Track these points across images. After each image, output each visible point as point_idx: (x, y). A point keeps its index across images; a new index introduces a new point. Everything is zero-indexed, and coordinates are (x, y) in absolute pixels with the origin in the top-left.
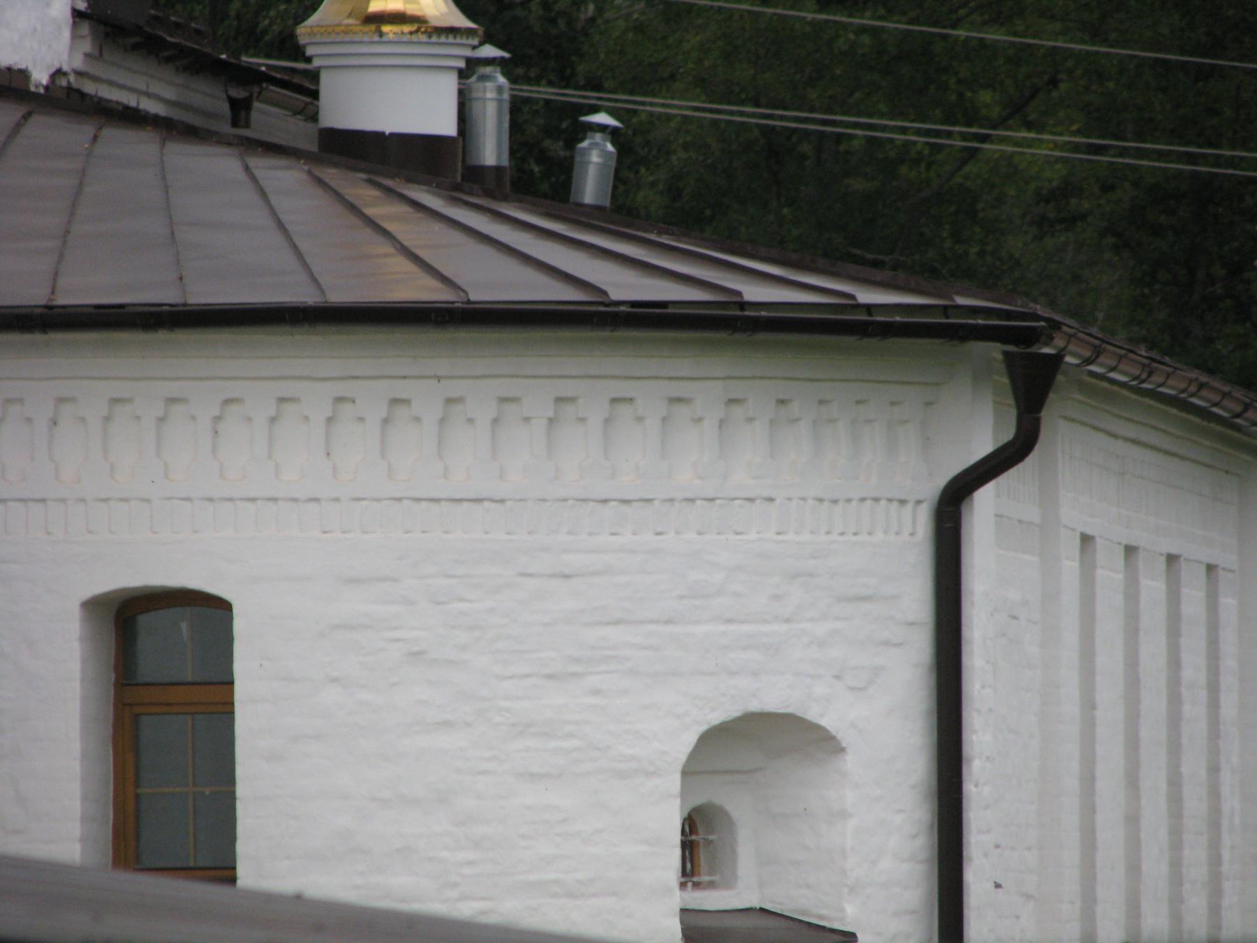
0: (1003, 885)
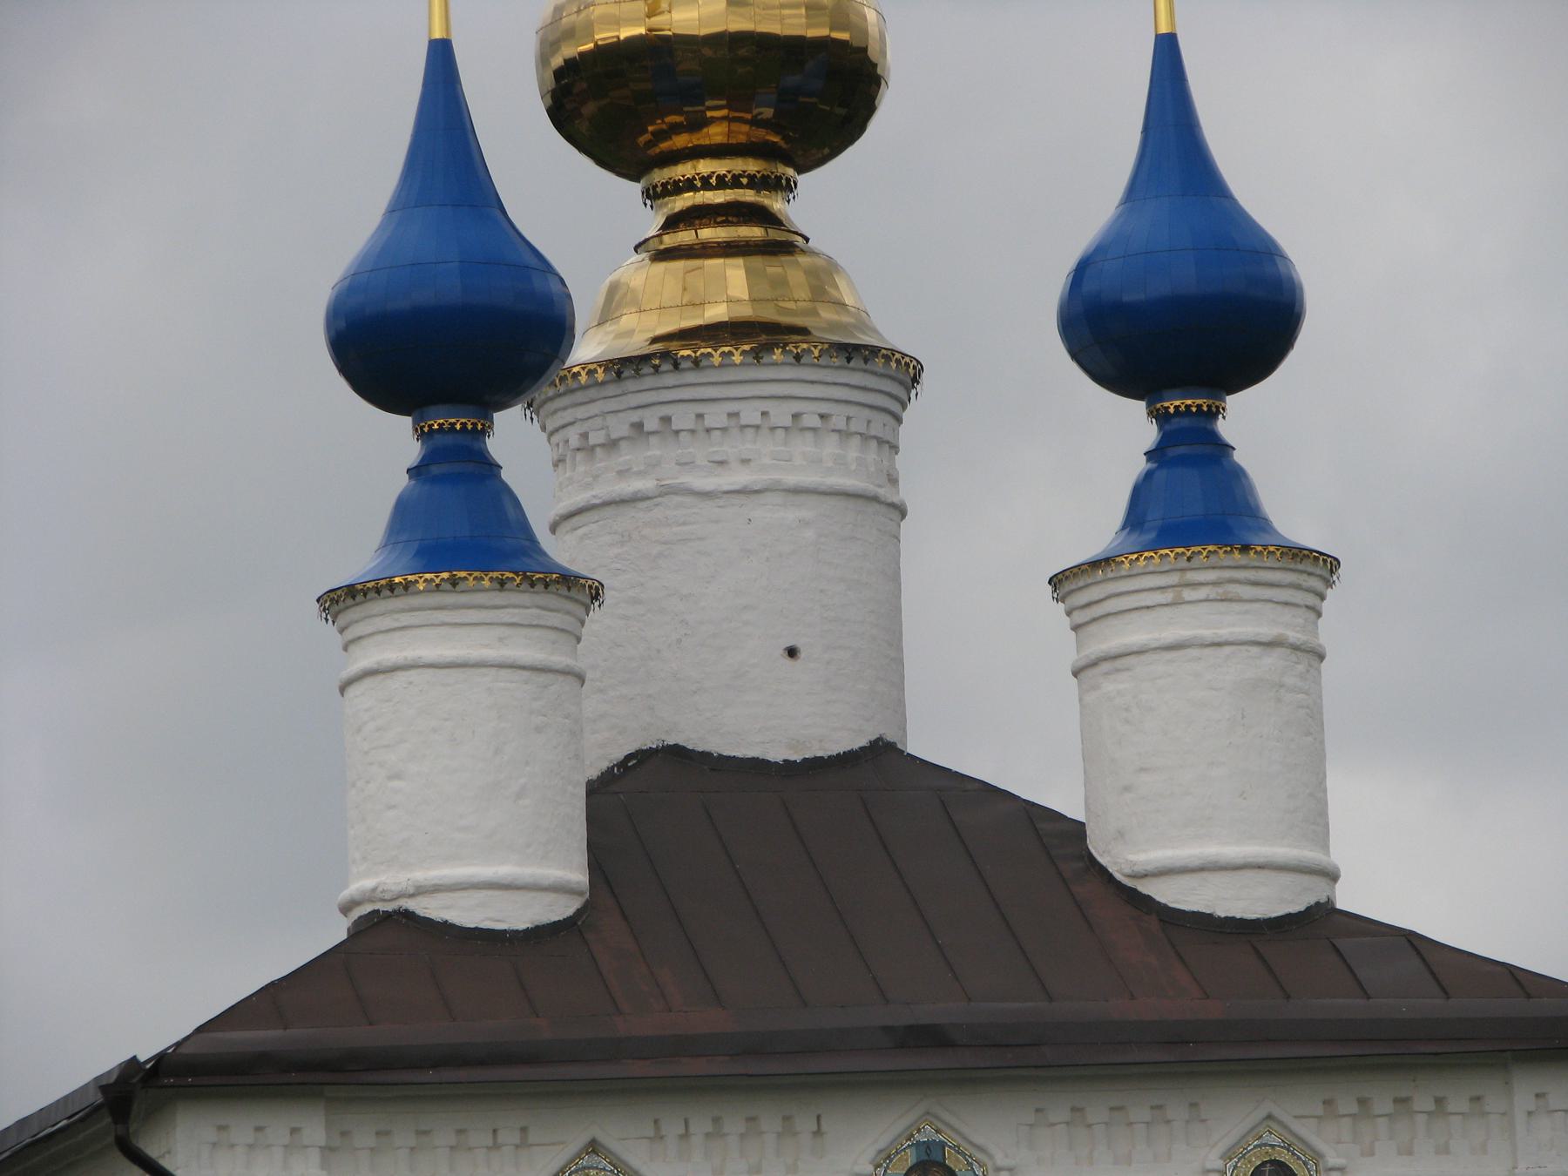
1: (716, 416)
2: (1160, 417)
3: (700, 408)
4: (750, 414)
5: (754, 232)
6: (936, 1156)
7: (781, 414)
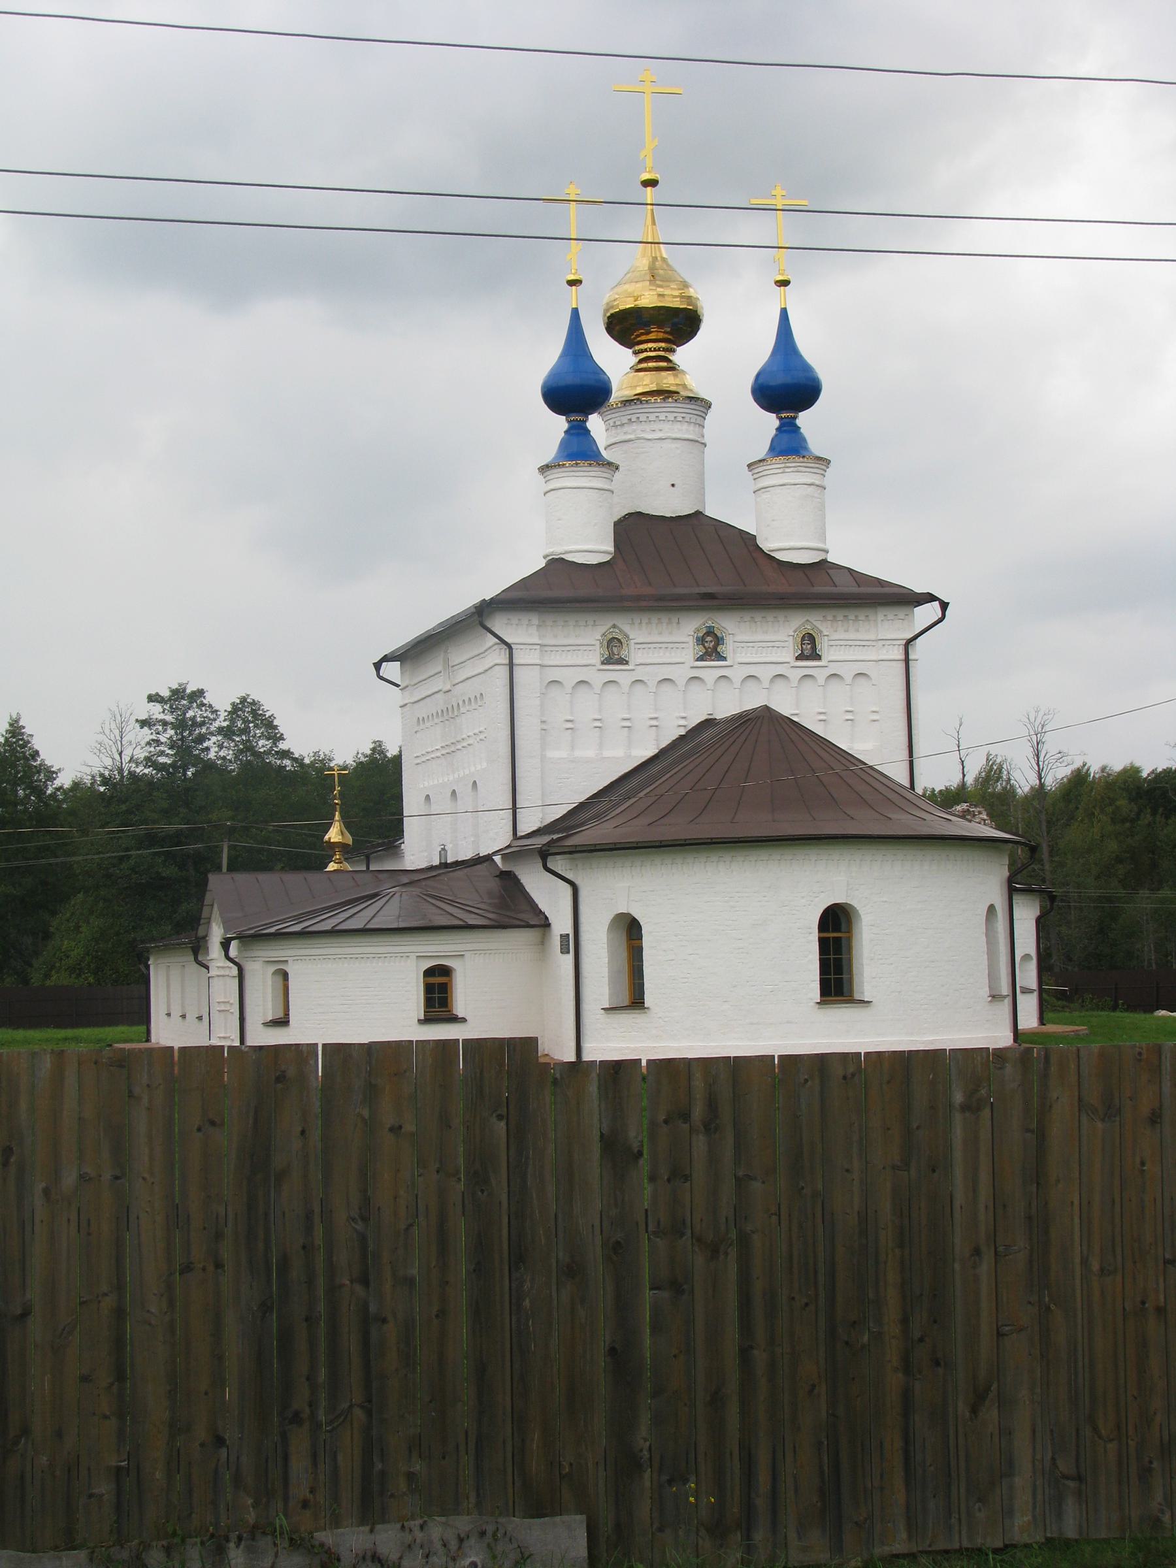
0: (651, 1007)
1: (652, 417)
2: (780, 419)
3: (647, 415)
4: (662, 417)
5: (664, 364)
6: (712, 630)
7: (671, 417)
